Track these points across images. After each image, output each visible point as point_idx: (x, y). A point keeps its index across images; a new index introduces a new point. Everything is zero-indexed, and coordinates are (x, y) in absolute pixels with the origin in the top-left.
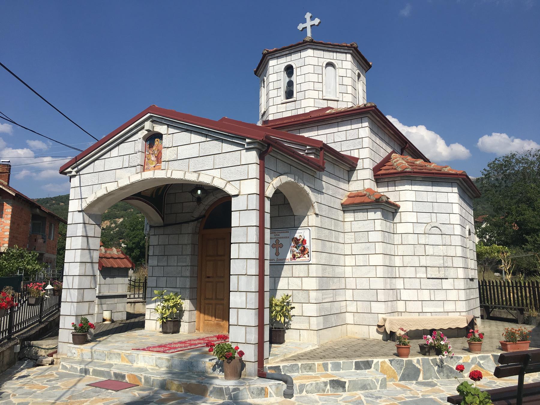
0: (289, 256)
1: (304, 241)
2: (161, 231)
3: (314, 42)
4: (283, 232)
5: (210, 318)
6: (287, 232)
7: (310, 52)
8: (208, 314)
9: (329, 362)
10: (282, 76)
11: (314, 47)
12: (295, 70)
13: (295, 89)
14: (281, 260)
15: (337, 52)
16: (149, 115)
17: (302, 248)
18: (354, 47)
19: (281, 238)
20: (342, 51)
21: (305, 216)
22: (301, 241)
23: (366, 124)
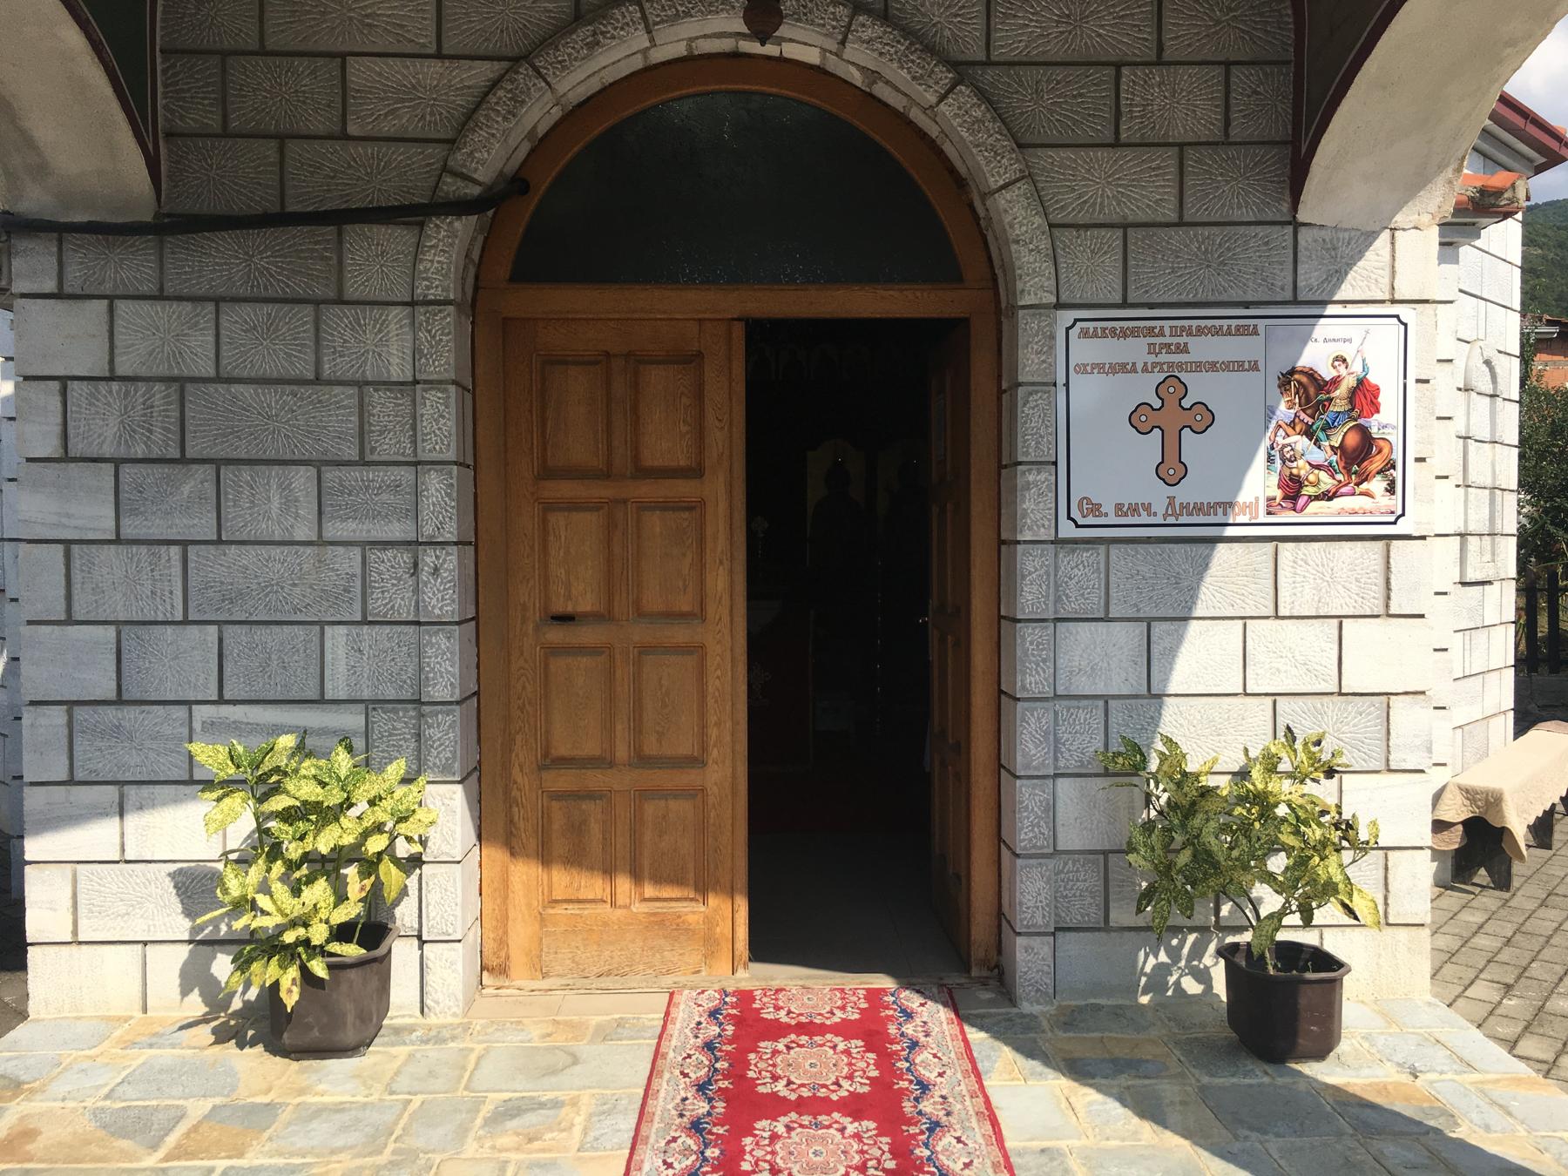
0: (1259, 484)
1: (1364, 395)
2: (133, 266)
4: (1217, 332)
5: (594, 886)
6: (1240, 331)
8: (576, 859)
14: (1199, 508)
17: (1353, 440)
19: (1198, 367)
21: (1371, 236)
22: (1341, 392)
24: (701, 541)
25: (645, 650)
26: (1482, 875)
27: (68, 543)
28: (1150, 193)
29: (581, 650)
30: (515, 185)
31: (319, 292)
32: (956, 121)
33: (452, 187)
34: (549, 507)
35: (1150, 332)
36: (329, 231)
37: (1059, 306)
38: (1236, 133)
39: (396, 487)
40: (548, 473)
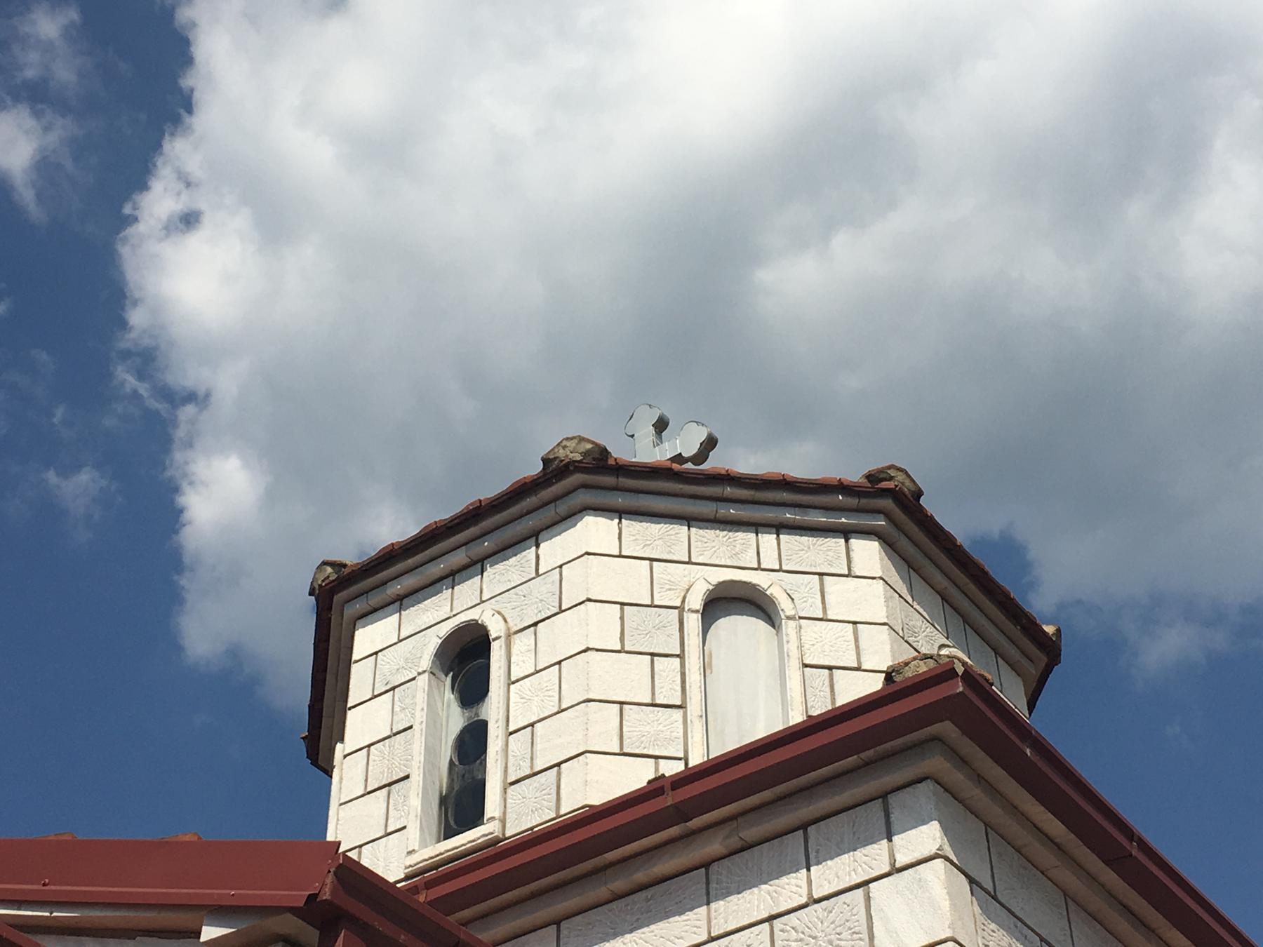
7: (595, 530)
10: (421, 699)
11: (620, 500)
12: (497, 651)
15: (780, 528)
18: (895, 494)
23: (926, 837)
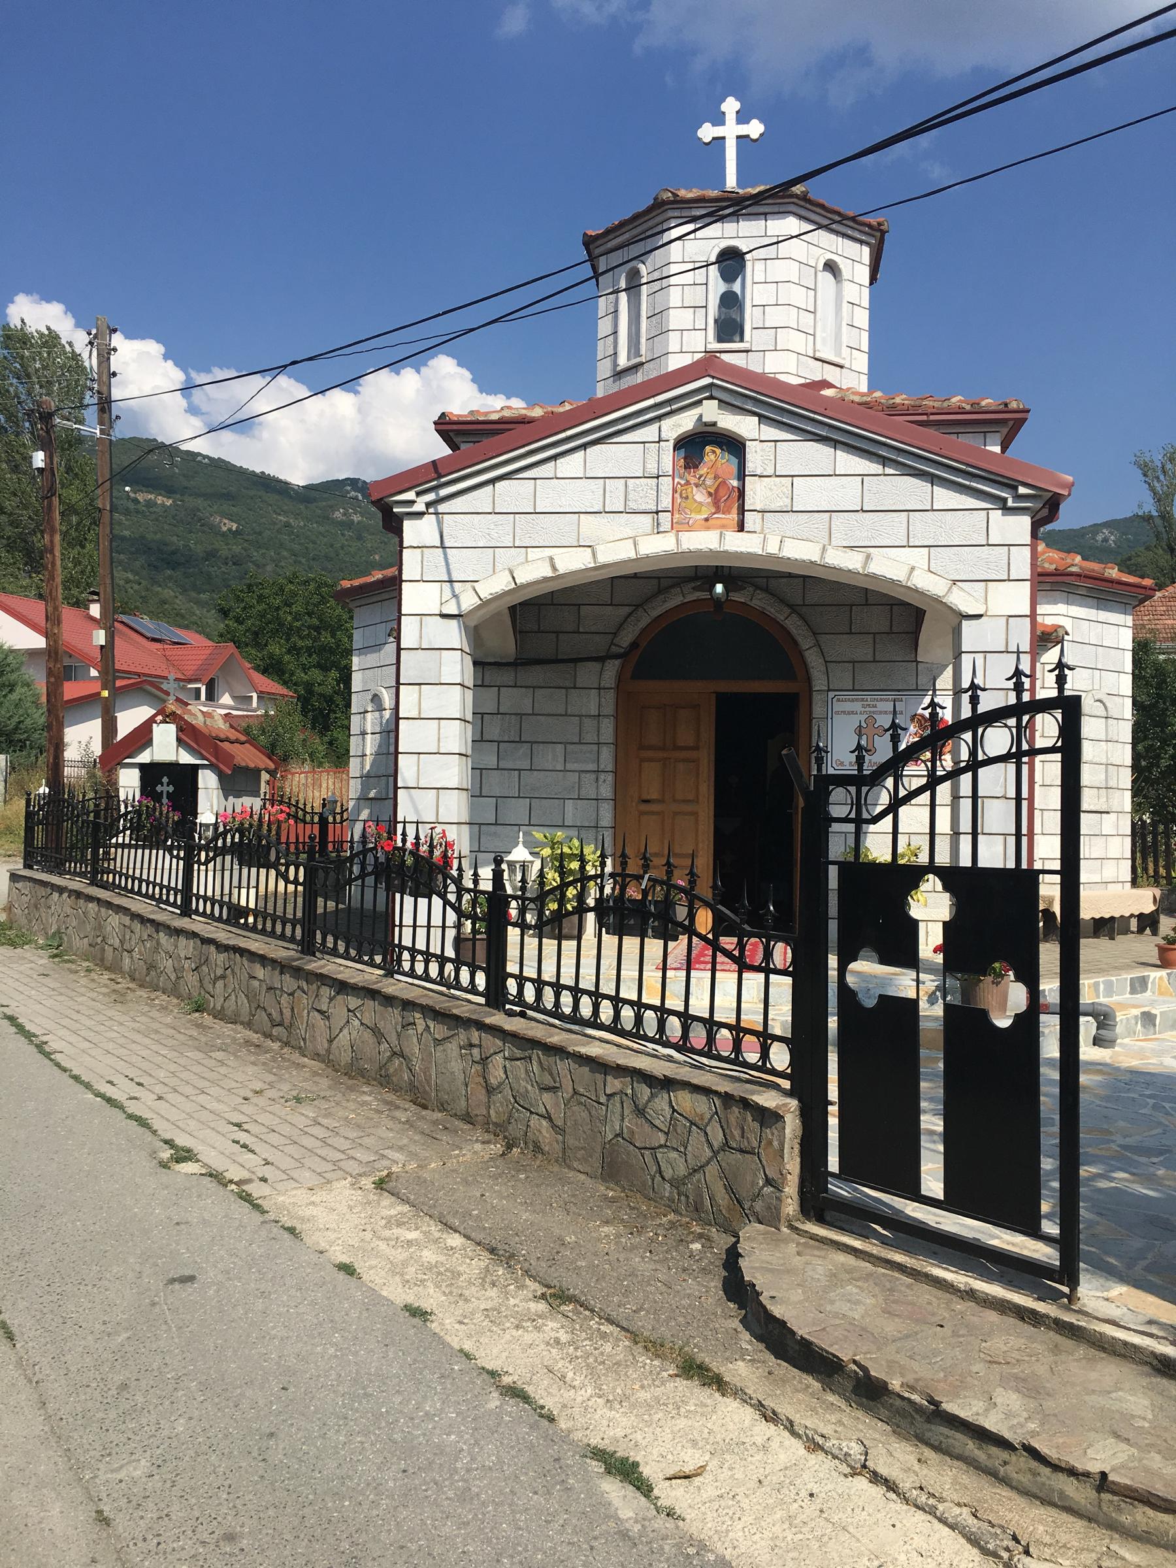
2: (507, 676)
3: (809, 201)
9: (1101, 980)
13: (751, 318)
16: (707, 381)
19: (881, 713)
20: (857, 235)
24: (698, 774)
25: (676, 814)
26: (1148, 931)
27: (481, 769)
28: (863, 650)
29: (653, 813)
30: (634, 645)
31: (568, 684)
32: (793, 624)
33: (614, 649)
34: (642, 760)
35: (863, 700)
36: (572, 665)
37: (829, 690)
38: (895, 629)
39: (591, 752)
40: (642, 747)
